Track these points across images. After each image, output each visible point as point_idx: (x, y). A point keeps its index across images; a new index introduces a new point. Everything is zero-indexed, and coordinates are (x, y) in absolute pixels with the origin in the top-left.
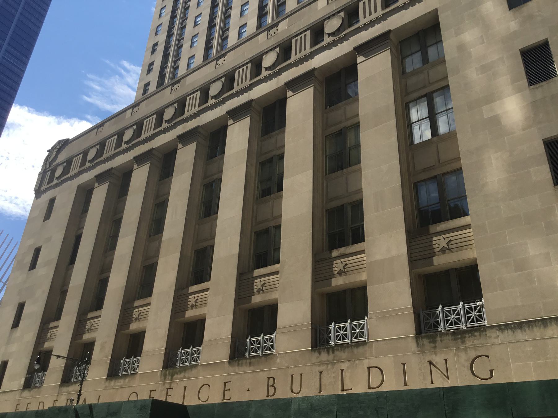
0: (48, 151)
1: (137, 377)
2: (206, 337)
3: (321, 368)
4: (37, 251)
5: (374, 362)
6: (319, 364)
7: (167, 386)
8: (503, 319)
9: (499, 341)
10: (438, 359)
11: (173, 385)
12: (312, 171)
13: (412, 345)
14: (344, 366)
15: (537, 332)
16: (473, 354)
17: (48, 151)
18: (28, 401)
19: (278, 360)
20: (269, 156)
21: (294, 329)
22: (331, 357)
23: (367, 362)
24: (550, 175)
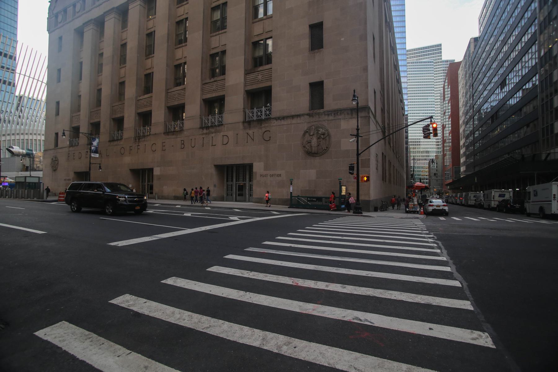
0: (49, 2)
1: (123, 140)
2: (153, 122)
3: (204, 136)
4: (59, 70)
5: (225, 133)
6: (203, 134)
7: (137, 144)
8: (278, 115)
9: (275, 124)
10: (250, 132)
11: (140, 144)
12: (202, 31)
13: (241, 126)
14: (213, 135)
15: (289, 121)
16: (264, 130)
17: (49, 2)
18: (73, 152)
19: (185, 133)
20: (181, 18)
21: (174, 282)
22: (208, 131)
23: (222, 134)
24: (308, 105)
